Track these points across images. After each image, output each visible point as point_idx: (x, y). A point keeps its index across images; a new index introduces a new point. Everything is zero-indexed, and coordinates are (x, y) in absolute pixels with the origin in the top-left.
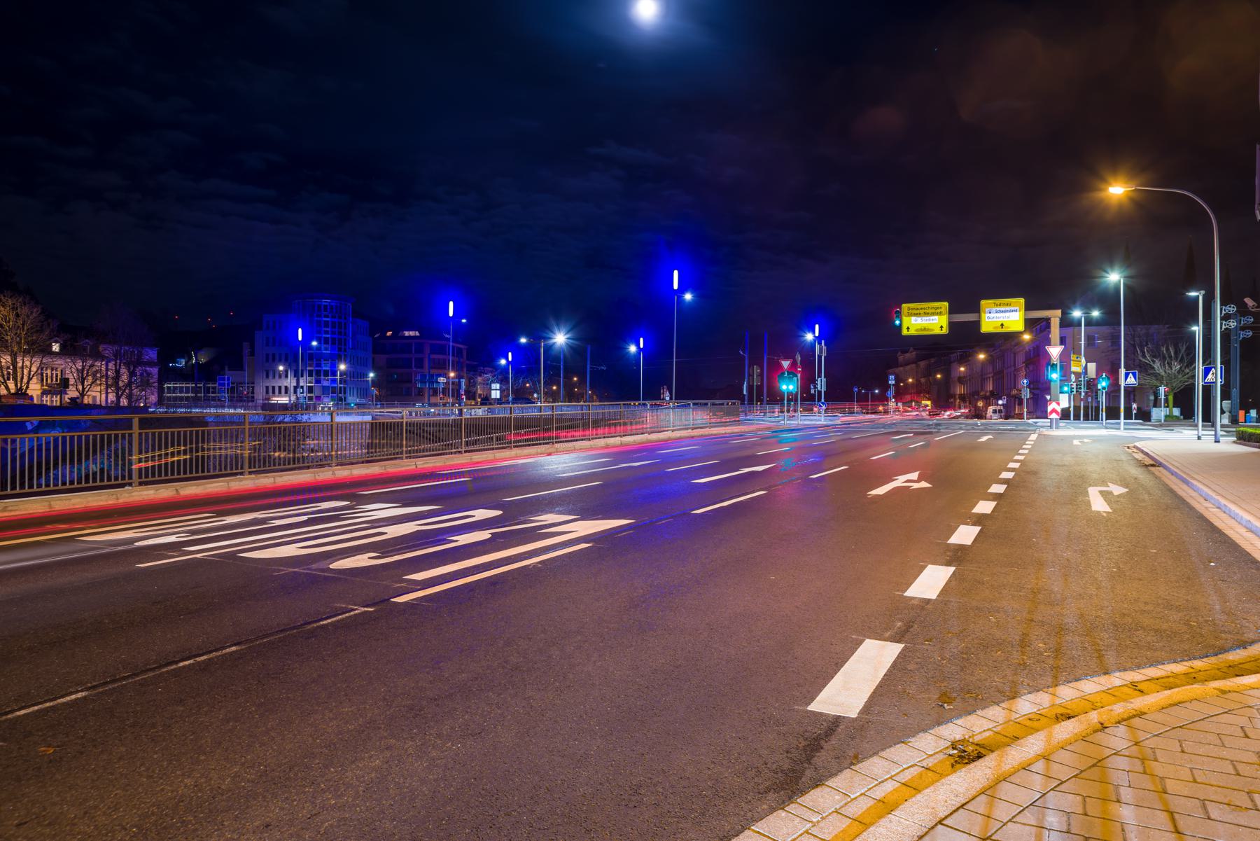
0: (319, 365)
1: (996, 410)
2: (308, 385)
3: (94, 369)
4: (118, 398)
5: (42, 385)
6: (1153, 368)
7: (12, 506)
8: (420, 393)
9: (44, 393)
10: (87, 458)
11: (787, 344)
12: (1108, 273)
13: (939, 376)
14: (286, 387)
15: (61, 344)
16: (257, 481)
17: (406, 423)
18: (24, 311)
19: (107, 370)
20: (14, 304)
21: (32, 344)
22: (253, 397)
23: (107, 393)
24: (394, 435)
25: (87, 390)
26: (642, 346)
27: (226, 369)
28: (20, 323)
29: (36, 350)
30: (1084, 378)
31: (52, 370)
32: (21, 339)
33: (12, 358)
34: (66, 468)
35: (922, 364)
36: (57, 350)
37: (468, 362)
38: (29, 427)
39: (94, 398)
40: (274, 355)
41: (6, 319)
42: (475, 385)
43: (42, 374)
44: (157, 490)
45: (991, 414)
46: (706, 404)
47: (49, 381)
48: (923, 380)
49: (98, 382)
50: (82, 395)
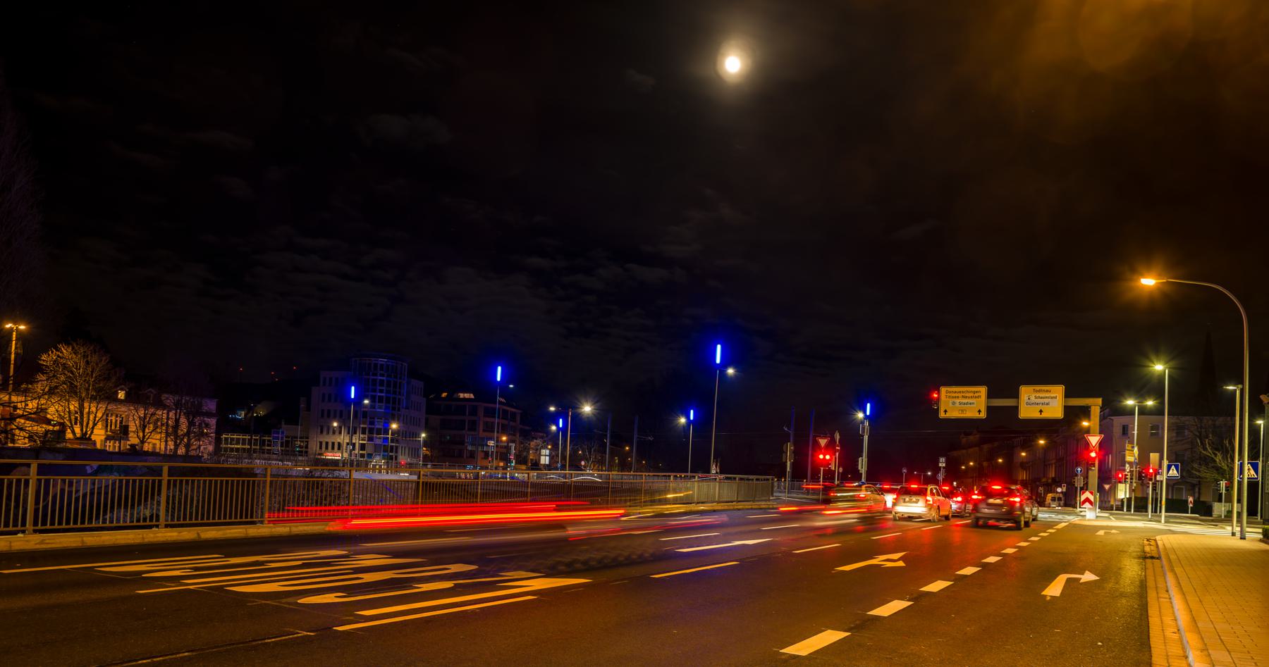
0: (372, 423)
1: (1055, 498)
2: (361, 442)
3: (155, 418)
4: (177, 446)
5: (107, 431)
6: (1215, 461)
7: (49, 539)
8: (472, 455)
9: (108, 438)
10: (139, 504)
11: (835, 419)
12: (1153, 363)
13: (1000, 461)
14: (339, 443)
15: (126, 392)
16: (273, 530)
17: (423, 482)
18: (95, 358)
19: (168, 419)
20: (85, 352)
21: (99, 391)
22: (306, 452)
23: (166, 441)
24: (439, 495)
25: (147, 437)
26: (692, 418)
27: (283, 423)
28: (90, 369)
29: (102, 396)
30: (1136, 468)
31: (117, 416)
32: (89, 386)
33: (79, 404)
34: (120, 512)
35: (986, 447)
36: (123, 398)
37: (521, 426)
38: (89, 471)
39: (155, 444)
40: (329, 411)
41: (77, 366)
42: (527, 449)
43: (107, 421)
44: (180, 533)
45: (1050, 501)
46: (735, 478)
47: (113, 427)
48: (985, 464)
49: (159, 430)
50: (143, 442)
